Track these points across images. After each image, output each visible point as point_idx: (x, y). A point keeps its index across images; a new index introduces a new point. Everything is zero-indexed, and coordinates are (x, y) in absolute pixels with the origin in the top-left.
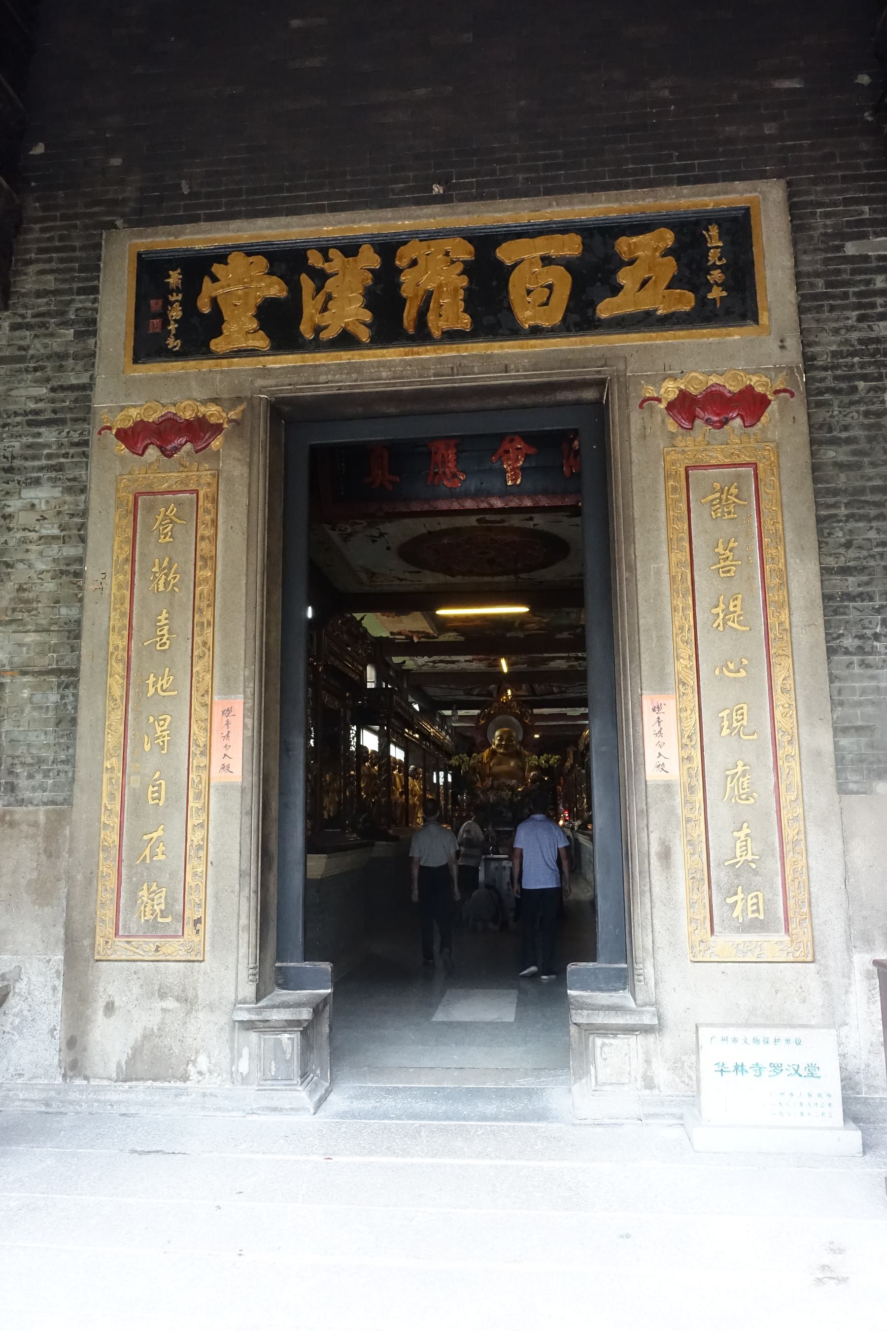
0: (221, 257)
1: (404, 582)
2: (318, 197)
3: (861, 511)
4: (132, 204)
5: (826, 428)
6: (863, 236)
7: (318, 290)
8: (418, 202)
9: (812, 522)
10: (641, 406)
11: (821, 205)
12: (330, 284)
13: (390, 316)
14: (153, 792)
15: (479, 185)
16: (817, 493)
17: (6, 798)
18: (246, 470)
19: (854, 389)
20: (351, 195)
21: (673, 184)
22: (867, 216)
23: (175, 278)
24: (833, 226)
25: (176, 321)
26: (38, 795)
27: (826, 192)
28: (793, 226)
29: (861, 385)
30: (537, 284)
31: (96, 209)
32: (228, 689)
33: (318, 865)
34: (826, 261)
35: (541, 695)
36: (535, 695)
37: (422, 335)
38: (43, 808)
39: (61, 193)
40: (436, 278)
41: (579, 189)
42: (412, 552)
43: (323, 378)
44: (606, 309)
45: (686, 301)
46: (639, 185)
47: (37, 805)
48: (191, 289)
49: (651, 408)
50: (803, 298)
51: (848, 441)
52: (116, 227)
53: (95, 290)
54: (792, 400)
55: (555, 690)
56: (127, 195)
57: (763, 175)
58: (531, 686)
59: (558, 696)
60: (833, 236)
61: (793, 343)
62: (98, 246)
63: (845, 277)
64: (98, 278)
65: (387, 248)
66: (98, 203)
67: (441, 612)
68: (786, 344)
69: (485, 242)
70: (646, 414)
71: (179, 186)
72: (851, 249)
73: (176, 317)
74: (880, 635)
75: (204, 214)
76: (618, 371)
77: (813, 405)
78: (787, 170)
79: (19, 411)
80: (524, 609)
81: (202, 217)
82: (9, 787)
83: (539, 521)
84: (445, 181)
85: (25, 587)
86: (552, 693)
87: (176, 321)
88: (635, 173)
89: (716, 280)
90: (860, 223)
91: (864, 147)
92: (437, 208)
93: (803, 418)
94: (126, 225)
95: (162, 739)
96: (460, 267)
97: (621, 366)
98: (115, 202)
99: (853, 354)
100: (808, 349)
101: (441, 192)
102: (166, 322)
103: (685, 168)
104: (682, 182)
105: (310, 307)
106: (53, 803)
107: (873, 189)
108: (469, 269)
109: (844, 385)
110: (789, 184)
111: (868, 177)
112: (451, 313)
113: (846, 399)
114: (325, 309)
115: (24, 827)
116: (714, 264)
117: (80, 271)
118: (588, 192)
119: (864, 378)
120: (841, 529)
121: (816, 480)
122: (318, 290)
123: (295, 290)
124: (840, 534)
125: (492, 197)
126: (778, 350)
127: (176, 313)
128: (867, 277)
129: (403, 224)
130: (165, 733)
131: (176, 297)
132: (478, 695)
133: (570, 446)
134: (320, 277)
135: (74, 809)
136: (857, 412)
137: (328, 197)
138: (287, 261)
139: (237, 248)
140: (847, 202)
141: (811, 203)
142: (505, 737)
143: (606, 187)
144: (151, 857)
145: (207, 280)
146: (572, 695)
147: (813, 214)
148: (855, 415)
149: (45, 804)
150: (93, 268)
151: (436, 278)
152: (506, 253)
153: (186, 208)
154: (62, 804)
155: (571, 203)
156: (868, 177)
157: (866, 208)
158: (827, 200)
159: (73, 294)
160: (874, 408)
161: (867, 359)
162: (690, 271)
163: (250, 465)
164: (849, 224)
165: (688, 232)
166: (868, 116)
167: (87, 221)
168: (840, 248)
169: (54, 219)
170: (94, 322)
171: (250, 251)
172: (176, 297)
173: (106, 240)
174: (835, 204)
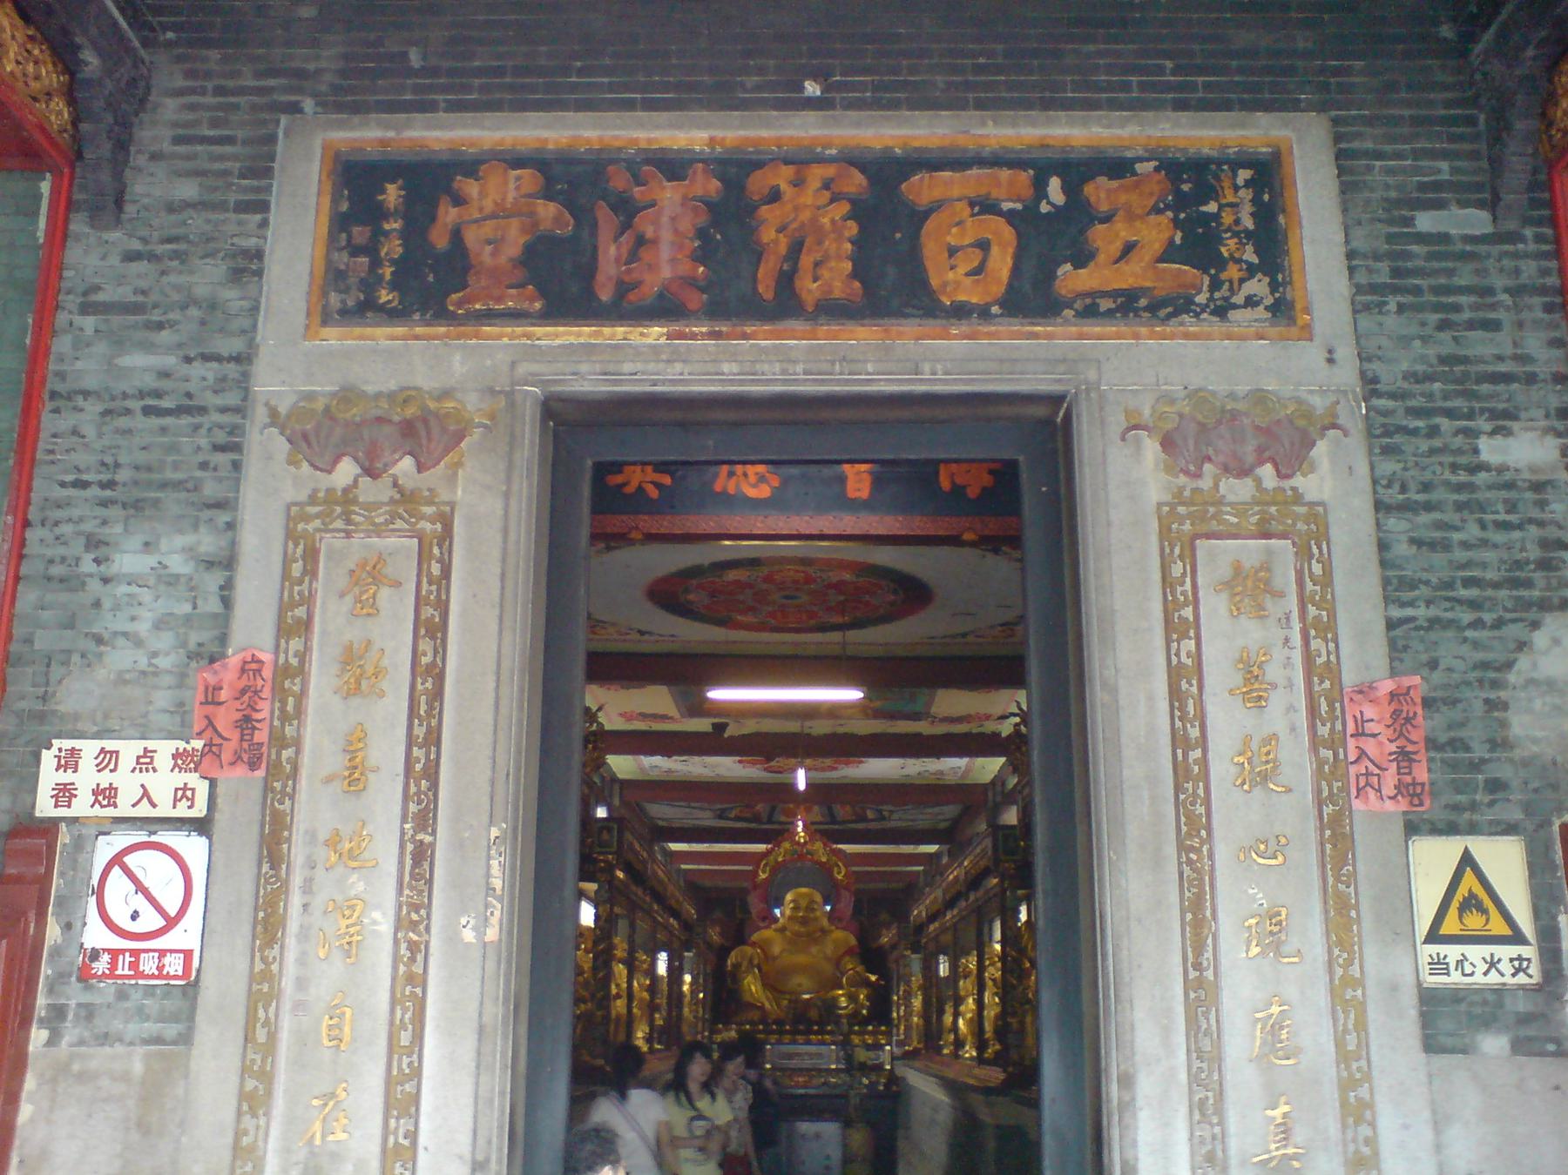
0: (470, 166)
1: (646, 637)
2: (626, 88)
3: (1449, 615)
4: (328, 77)
5: (1397, 486)
6: (1439, 205)
9: (1380, 626)
10: (1123, 439)
11: (1379, 156)
14: (330, 1027)
15: (877, 87)
16: (1386, 582)
17: (77, 1031)
18: (498, 506)
19: (1434, 431)
20: (677, 87)
22: (1447, 177)
23: (392, 194)
24: (1398, 188)
25: (393, 262)
26: (133, 1029)
27: (1392, 139)
28: (1342, 183)
29: (1445, 423)
31: (272, 82)
34: (1390, 238)
35: (844, 822)
36: (834, 822)
37: (784, 305)
38: (140, 1050)
39: (214, 54)
40: (812, 221)
41: (1027, 105)
42: (668, 594)
43: (627, 367)
44: (1071, 279)
46: (1114, 105)
47: (131, 1044)
48: (419, 214)
49: (1138, 441)
50: (1359, 289)
51: (1429, 507)
52: (301, 111)
53: (263, 207)
54: (1347, 440)
55: (870, 814)
56: (324, 64)
57: (1295, 106)
58: (830, 808)
59: (872, 826)
60: (1398, 203)
61: (1346, 353)
62: (272, 139)
63: (1419, 263)
64: (268, 189)
65: (736, 169)
66: (274, 73)
67: (718, 694)
68: (1335, 356)
69: (888, 171)
71: (404, 55)
72: (1425, 222)
73: (401, 253)
74: (1481, 803)
75: (446, 101)
76: (1087, 382)
77: (1377, 451)
78: (1328, 97)
79: (130, 391)
80: (853, 695)
81: (443, 105)
82: (83, 1013)
83: (884, 556)
84: (818, 75)
85: (127, 676)
86: (864, 819)
87: (393, 262)
88: (1110, 87)
89: (1222, 240)
90: (1437, 186)
91: (1440, 77)
92: (811, 116)
93: (1363, 469)
94: (319, 109)
95: (347, 939)
96: (845, 207)
97: (1092, 375)
98: (300, 74)
99: (1430, 378)
100: (1367, 366)
102: (376, 263)
104: (1181, 106)
105: (610, 254)
106: (158, 1040)
107: (1452, 139)
108: (860, 211)
109: (1421, 424)
110: (1336, 121)
111: (1444, 121)
112: (834, 274)
113: (1424, 445)
114: (633, 257)
115: (105, 1082)
117: (243, 176)
119: (1450, 414)
120: (1422, 640)
121: (1383, 564)
122: (626, 226)
124: (1421, 648)
125: (894, 105)
126: (1323, 363)
127: (393, 248)
128: (1450, 265)
130: (352, 930)
131: (394, 225)
132: (738, 819)
133: (1002, 487)
135: (195, 1052)
136: (1441, 464)
137: (644, 88)
138: (571, 179)
140: (1417, 154)
141: (1366, 154)
142: (803, 903)
143: (1068, 105)
144: (324, 1136)
146: (899, 824)
147: (1369, 169)
148: (1438, 470)
149: (146, 1042)
150: (261, 170)
151: (812, 221)
152: (921, 188)
153: (417, 89)
154: (175, 1043)
155: (1014, 125)
156: (1444, 121)
157: (1444, 165)
158: (1388, 148)
159: (227, 210)
160: (1463, 460)
161: (1451, 387)
162: (1199, 246)
163: (507, 496)
164: (1422, 187)
165: (1190, 178)
166: (1446, 31)
167: (255, 99)
168: (1409, 222)
169: (203, 92)
170: (259, 255)
171: (517, 161)
172: (394, 225)
173: (286, 134)
174: (1399, 156)
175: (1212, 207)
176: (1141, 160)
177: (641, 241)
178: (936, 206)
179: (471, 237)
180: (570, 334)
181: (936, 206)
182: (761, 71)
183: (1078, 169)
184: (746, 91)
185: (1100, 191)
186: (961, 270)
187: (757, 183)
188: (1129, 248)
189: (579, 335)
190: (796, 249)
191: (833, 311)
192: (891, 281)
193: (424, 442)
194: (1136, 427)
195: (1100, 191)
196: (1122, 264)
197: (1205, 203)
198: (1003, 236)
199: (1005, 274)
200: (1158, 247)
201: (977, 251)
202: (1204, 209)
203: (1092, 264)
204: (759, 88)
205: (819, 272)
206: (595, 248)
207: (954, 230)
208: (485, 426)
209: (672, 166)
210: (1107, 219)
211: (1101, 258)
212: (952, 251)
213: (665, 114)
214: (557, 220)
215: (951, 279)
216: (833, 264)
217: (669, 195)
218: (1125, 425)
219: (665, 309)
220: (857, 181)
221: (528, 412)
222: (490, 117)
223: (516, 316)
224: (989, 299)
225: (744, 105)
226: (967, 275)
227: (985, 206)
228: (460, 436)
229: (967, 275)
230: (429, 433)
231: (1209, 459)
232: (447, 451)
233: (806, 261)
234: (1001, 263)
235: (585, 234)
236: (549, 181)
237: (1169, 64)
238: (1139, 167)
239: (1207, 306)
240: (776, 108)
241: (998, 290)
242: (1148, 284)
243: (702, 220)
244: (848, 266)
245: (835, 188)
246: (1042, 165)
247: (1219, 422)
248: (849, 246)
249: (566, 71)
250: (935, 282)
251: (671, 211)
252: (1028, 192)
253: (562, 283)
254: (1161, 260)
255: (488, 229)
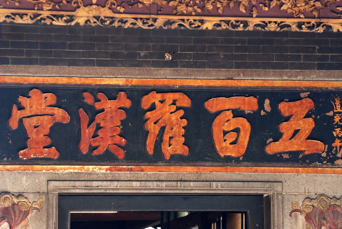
0: (24, 91)
7: (91, 121)
8: (156, 65)
10: (290, 216)
12: (99, 118)
13: (136, 148)
21: (315, 69)
30: (230, 132)
32: (236, 155)
33: (25, 56)
37: (157, 158)
40: (167, 118)
44: (273, 148)
45: (319, 146)
49: (296, 217)
65: (136, 94)
70: (293, 220)
81: (10, 61)
96: (182, 113)
97: (279, 189)
101: (171, 59)
103: (323, 58)
105: (87, 132)
108: (188, 114)
112: (176, 146)
116: (337, 123)
118: (263, 69)
122: (91, 121)
123: (75, 118)
129: (119, 167)
134: (93, 113)
138: (69, 97)
139: (35, 86)
145: (15, 107)
151: (167, 118)
152: (213, 105)
171: (45, 89)
175: (331, 114)
176: (303, 92)
177: (99, 127)
178: (219, 113)
179: (27, 123)
180: (71, 169)
181: (219, 113)
182: (147, 48)
183: (278, 96)
184: (140, 57)
185: (284, 107)
186: (228, 142)
187: (146, 102)
188: (296, 132)
189: (74, 169)
190: (163, 129)
191: (177, 160)
192: (200, 147)
193: (13, 217)
194: (296, 211)
195: (284, 107)
196: (293, 140)
197: (329, 112)
198: (245, 125)
199: (246, 143)
200: (308, 132)
201: (235, 133)
202: (328, 114)
203: (281, 140)
204: (145, 56)
205: (171, 143)
206: (80, 129)
207: (226, 124)
208: (37, 209)
209: (112, 93)
210: (287, 119)
211: (284, 136)
212: (225, 133)
213: (107, 69)
214: (64, 118)
215: (225, 147)
216: (177, 138)
217: (109, 105)
218: (291, 209)
219: (107, 158)
220: (185, 102)
221: (54, 203)
222: (33, 68)
223: (47, 161)
224: (239, 155)
225: (139, 65)
226: (231, 144)
227: (237, 113)
228: (26, 213)
229: (231, 144)
230: (15, 213)
231: (324, 225)
232: (22, 220)
233: (166, 138)
234: (245, 139)
235: (75, 122)
236: (59, 98)
237: (317, 47)
238: (302, 95)
239: (326, 158)
240: (153, 66)
241: (243, 151)
242: (303, 149)
243: (124, 117)
244: (183, 139)
245: (178, 104)
246: (260, 94)
247: (328, 209)
248: (183, 130)
249: (64, 45)
250: (218, 148)
251: (112, 109)
252: (256, 107)
253: (66, 146)
254: (308, 138)
255: (34, 121)
